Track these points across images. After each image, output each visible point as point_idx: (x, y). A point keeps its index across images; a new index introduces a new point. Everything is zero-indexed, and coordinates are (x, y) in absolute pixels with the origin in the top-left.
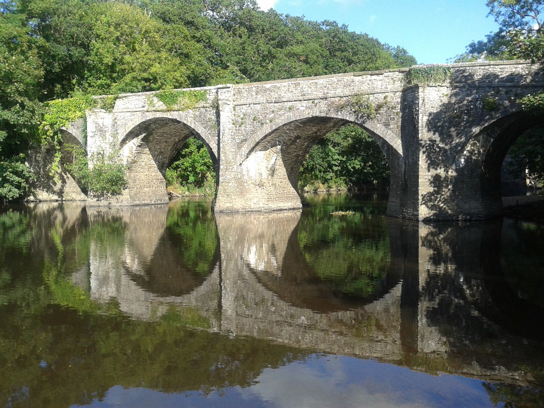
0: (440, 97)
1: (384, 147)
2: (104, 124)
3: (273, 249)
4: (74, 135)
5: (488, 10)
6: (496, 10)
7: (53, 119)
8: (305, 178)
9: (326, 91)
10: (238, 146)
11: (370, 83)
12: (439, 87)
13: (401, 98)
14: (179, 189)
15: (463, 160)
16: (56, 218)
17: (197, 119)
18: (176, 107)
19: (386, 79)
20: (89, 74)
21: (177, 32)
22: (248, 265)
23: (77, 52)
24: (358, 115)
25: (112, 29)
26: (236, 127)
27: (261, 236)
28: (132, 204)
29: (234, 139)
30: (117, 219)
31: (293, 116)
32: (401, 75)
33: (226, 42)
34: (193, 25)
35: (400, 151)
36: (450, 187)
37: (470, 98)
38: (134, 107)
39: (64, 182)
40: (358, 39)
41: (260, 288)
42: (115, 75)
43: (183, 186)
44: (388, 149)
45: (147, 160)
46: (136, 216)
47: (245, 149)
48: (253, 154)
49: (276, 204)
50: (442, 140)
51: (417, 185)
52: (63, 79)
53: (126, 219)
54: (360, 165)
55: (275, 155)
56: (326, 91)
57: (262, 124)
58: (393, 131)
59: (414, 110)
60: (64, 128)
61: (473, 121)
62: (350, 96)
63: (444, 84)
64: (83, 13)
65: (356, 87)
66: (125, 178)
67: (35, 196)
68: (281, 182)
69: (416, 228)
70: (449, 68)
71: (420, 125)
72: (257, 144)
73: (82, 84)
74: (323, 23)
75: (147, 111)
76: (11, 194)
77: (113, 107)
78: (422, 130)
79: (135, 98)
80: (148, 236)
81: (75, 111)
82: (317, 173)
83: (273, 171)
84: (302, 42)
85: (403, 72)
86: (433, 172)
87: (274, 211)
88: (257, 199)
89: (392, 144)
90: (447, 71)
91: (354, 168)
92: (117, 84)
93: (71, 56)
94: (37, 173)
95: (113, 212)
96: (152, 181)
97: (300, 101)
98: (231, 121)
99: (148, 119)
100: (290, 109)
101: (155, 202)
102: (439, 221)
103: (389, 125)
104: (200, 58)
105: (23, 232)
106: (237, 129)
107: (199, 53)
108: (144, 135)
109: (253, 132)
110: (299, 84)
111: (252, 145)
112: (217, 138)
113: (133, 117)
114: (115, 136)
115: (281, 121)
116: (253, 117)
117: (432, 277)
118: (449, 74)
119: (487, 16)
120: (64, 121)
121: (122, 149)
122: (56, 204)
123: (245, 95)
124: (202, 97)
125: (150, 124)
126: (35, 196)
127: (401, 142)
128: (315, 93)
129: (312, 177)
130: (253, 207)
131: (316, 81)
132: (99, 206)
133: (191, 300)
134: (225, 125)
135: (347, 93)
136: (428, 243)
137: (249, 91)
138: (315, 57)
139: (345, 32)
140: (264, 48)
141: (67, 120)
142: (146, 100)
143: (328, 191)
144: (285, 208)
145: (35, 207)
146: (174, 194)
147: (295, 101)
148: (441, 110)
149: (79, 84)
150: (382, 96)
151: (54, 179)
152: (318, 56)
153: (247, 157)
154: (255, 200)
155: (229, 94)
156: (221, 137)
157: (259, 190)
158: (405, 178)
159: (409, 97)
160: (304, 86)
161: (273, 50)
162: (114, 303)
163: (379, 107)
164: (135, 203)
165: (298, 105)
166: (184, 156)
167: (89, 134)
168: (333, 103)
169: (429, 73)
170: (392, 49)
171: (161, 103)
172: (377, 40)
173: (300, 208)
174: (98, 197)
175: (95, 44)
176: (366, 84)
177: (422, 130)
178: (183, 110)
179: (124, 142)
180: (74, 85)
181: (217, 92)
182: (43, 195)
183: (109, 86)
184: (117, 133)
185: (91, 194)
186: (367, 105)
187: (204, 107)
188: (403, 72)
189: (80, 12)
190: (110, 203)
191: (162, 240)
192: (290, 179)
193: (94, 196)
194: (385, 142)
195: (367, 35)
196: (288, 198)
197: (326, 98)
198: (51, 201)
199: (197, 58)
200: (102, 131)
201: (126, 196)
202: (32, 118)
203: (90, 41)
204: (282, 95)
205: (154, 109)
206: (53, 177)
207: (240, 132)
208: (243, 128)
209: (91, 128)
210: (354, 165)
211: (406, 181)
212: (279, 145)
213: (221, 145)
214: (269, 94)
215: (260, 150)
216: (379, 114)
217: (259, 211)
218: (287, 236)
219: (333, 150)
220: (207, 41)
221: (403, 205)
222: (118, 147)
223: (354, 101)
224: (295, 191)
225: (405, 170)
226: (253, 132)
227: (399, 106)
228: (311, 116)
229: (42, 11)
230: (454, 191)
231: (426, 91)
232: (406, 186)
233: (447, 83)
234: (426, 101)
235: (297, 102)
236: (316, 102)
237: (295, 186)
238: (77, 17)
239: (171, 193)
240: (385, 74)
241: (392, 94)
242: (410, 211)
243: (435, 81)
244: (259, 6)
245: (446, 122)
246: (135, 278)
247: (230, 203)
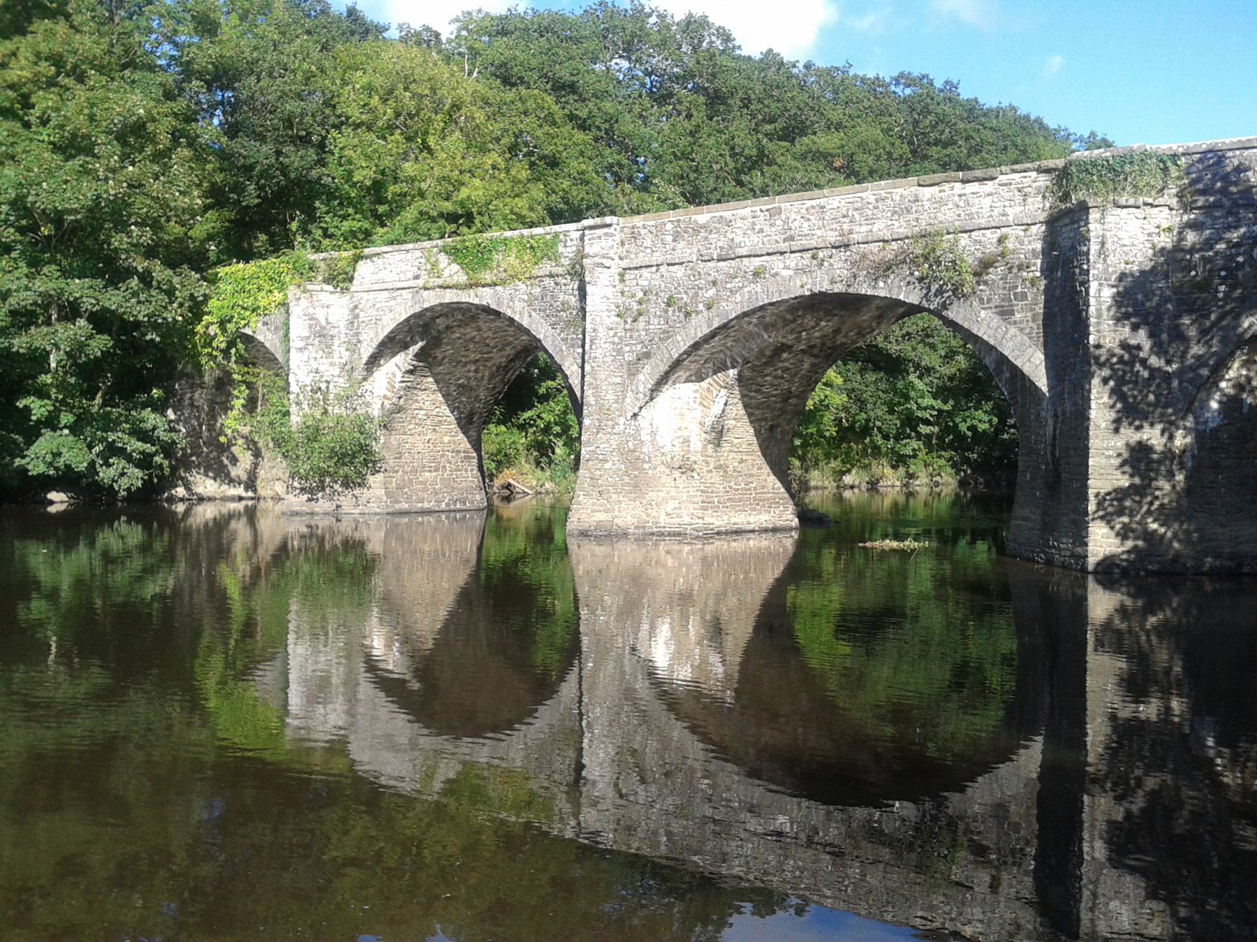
0: (1149, 235)
1: (1002, 372)
2: (330, 320)
3: (716, 631)
4: (268, 345)
7: (225, 311)
8: (847, 454)
9: (846, 227)
10: (629, 370)
11: (962, 204)
12: (1147, 208)
13: (1045, 240)
14: (530, 476)
15: (1214, 405)
16: (233, 540)
17: (537, 305)
18: (488, 277)
19: (1003, 191)
20: (324, 209)
21: (530, 104)
22: (651, 673)
23: (297, 158)
24: (929, 288)
25: (375, 101)
26: (626, 322)
27: (685, 599)
28: (390, 510)
30: (353, 546)
32: (1043, 180)
33: (659, 129)
34: (575, 93)
35: (1042, 383)
36: (1180, 477)
37: (1234, 236)
38: (398, 277)
39: (257, 454)
40: (985, 115)
41: (678, 731)
42: (382, 209)
43: (542, 469)
45: (431, 403)
46: (401, 538)
47: (646, 378)
48: (668, 394)
49: (725, 518)
50: (1159, 348)
51: (1084, 476)
52: (273, 221)
53: (375, 545)
54: (990, 421)
55: (723, 392)
56: (846, 227)
57: (688, 315)
58: (1021, 330)
59: (1077, 271)
60: (248, 331)
61: (1243, 299)
62: (907, 238)
63: (1161, 201)
64: (314, 68)
65: (925, 216)
66: (376, 447)
67: (188, 487)
68: (742, 461)
69: (1079, 592)
70: (1174, 157)
71: (1092, 310)
72: (676, 365)
73: (310, 233)
74: (897, 81)
75: (426, 289)
76: (124, 483)
77: (351, 279)
78: (1098, 324)
79: (398, 256)
80: (430, 586)
81: (270, 291)
82: (879, 440)
83: (718, 434)
84: (839, 126)
85: (1048, 171)
86: (1130, 435)
87: (718, 533)
88: (674, 504)
89: (1018, 363)
90: (1169, 164)
91: (972, 428)
92: (386, 229)
93: (284, 169)
94: (194, 434)
95: (346, 527)
96: (443, 456)
97: (782, 253)
98: (613, 307)
99: (426, 305)
100: (756, 274)
101: (448, 505)
102: (1135, 574)
103: (1012, 313)
104: (583, 167)
105: (149, 571)
106: (628, 327)
107: (582, 153)
109: (666, 335)
111: (663, 368)
112: (580, 350)
113: (393, 303)
114: (353, 347)
115: (732, 307)
116: (664, 297)
117: (1126, 733)
118: (1174, 172)
120: (248, 313)
121: (371, 379)
122: (240, 506)
123: (648, 243)
124: (546, 250)
125: (434, 318)
126: (188, 487)
127: (1042, 357)
128: (819, 233)
129: (865, 450)
131: (822, 201)
132: (312, 514)
133: (515, 748)
134: (598, 319)
135: (901, 230)
136: (1113, 638)
137: (658, 231)
138: (870, 160)
139: (950, 100)
140: (747, 144)
141: (254, 310)
142: (423, 261)
143: (906, 485)
144: (751, 527)
145: (187, 512)
146: (519, 487)
147: (768, 254)
148: (1153, 268)
149: (306, 232)
150: (992, 236)
151: (233, 449)
152: (878, 158)
153: (652, 399)
155: (610, 242)
156: (587, 347)
157: (682, 480)
158: (1053, 454)
159: (1064, 240)
160: (793, 216)
161: (770, 146)
162: (338, 747)
163: (986, 265)
164: (397, 506)
165: (776, 263)
166: (545, 398)
168: (864, 256)
169: (1120, 173)
170: (1075, 141)
171: (455, 267)
172: (1038, 121)
173: (791, 529)
174: (311, 491)
175: (341, 140)
176: (950, 206)
177: (1098, 324)
178: (503, 282)
179: (374, 361)
180: (294, 235)
181: (582, 239)
182: (206, 485)
183: (368, 234)
184: (359, 342)
185: (296, 484)
186: (953, 262)
187: (551, 276)
188: (1048, 171)
189: (305, 66)
190: (338, 506)
191: (465, 597)
192: (765, 453)
193: (302, 489)
194: (1003, 360)
195: (1014, 109)
196: (759, 502)
197: (847, 246)
198: (225, 499)
199: (575, 165)
200: (324, 336)
202: (165, 308)
203: (328, 132)
204: (737, 240)
205: (440, 282)
206: (230, 444)
207: (635, 335)
208: (641, 324)
209: (298, 328)
210: (975, 422)
211: (1056, 463)
212: (734, 367)
213: (587, 368)
214: (706, 238)
215: (688, 380)
216: (986, 283)
217: (679, 534)
218: (755, 598)
219: (920, 385)
220: (603, 127)
221: (1049, 527)
222: (358, 375)
223: (919, 251)
224: (779, 484)
225: (1055, 435)
226: (666, 335)
227: (1039, 261)
228: (807, 293)
229: (213, 63)
230: (1189, 491)
231: (1109, 219)
232: (1057, 475)
233: (1170, 198)
234: (1109, 245)
235: (774, 257)
236: (821, 255)
237: (780, 470)
238: (299, 77)
239: (510, 485)
240: (1001, 177)
241: (1019, 231)
242: (1066, 544)
243: (1136, 190)
244: (737, 43)
245: (1168, 300)
246: (389, 686)
247: (606, 511)
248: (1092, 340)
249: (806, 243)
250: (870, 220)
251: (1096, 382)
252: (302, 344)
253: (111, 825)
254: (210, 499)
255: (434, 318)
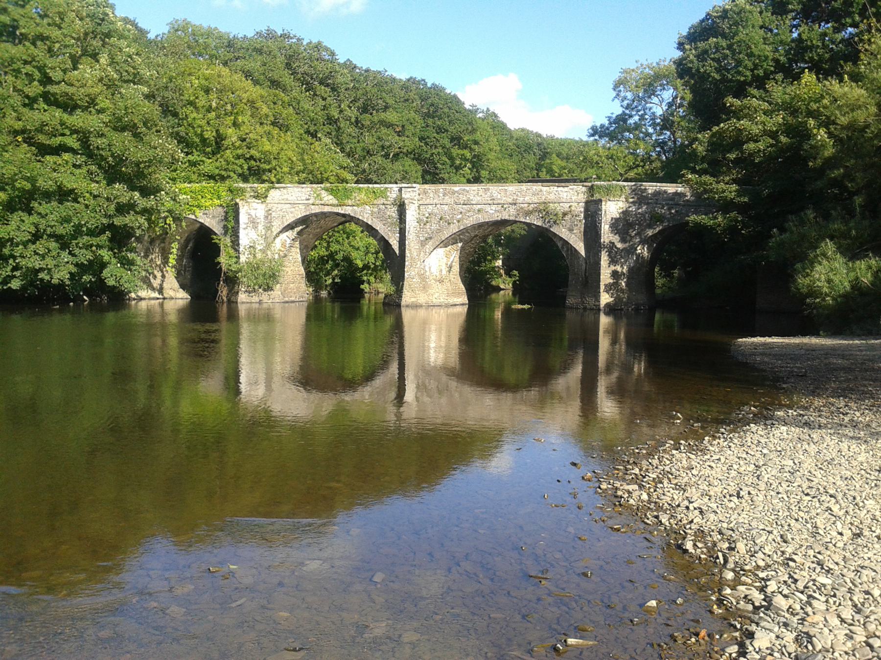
5: (614, 94)
6: (622, 94)
18: (350, 202)
31: (482, 218)
32: (584, 189)
35: (583, 253)
57: (449, 224)
86: (613, 268)
100: (479, 211)
102: (611, 310)
108: (301, 227)
110: (489, 189)
114: (268, 228)
115: (470, 222)
119: (613, 100)
124: (383, 194)
130: (436, 301)
154: (436, 295)
159: (592, 208)
163: (565, 214)
165: (488, 208)
168: (522, 208)
171: (331, 197)
178: (358, 205)
187: (384, 204)
196: (459, 295)
198: (150, 299)
201: (277, 292)
211: (586, 278)
226: (439, 231)
232: (587, 282)
233: (623, 198)
241: (576, 204)
248: (602, 240)
249: (499, 202)
250: (524, 196)
251: (603, 253)
252: (245, 226)
254: (144, 299)
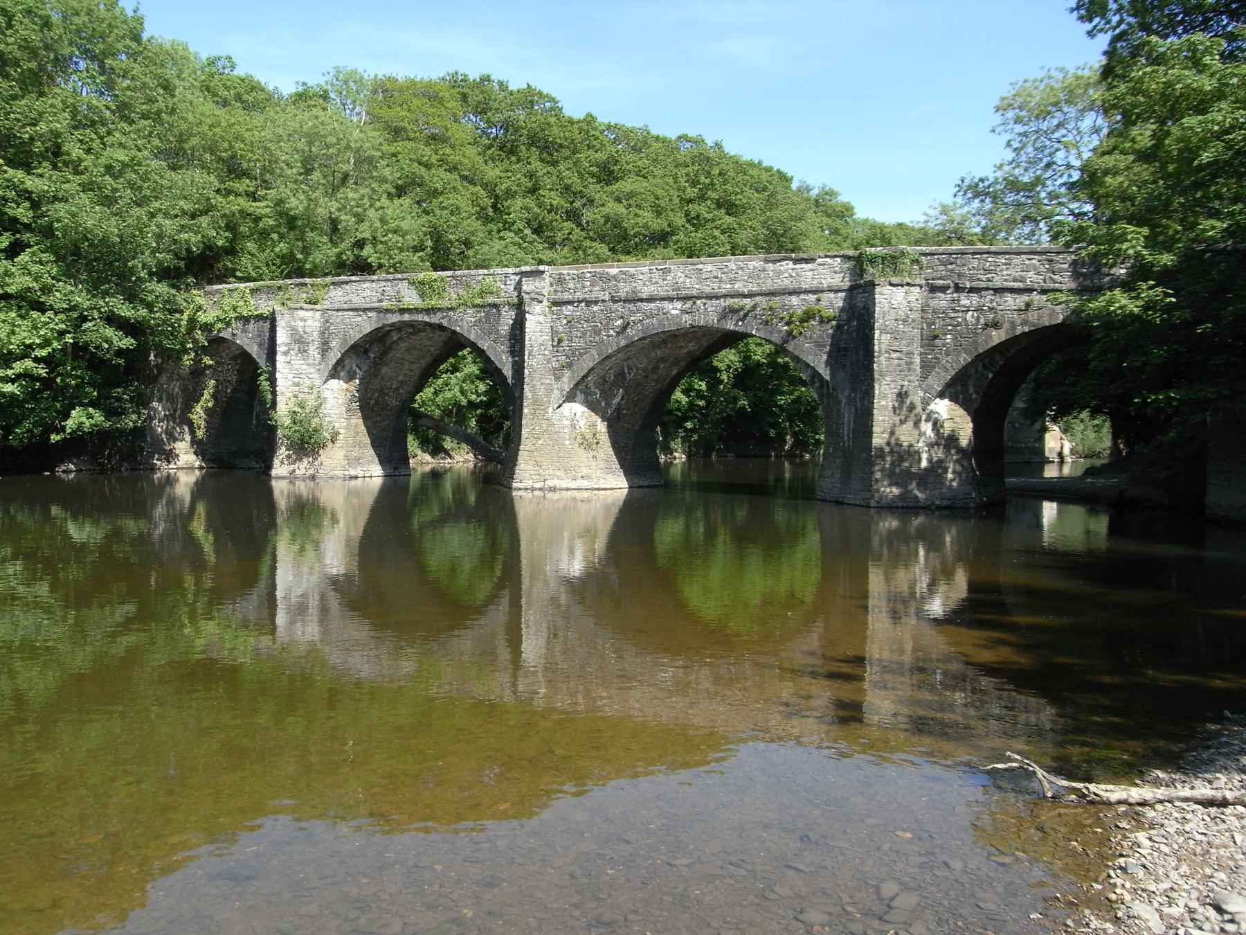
29: (549, 361)
38: (357, 304)
44: (958, 397)
165: (667, 306)
167: (280, 349)
209: (282, 336)
250: (733, 281)
253: (940, 278)
255: (389, 331)
